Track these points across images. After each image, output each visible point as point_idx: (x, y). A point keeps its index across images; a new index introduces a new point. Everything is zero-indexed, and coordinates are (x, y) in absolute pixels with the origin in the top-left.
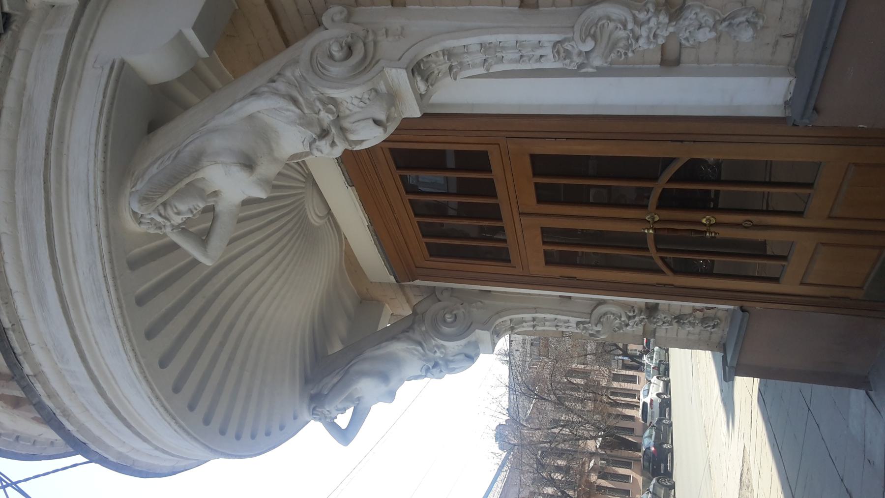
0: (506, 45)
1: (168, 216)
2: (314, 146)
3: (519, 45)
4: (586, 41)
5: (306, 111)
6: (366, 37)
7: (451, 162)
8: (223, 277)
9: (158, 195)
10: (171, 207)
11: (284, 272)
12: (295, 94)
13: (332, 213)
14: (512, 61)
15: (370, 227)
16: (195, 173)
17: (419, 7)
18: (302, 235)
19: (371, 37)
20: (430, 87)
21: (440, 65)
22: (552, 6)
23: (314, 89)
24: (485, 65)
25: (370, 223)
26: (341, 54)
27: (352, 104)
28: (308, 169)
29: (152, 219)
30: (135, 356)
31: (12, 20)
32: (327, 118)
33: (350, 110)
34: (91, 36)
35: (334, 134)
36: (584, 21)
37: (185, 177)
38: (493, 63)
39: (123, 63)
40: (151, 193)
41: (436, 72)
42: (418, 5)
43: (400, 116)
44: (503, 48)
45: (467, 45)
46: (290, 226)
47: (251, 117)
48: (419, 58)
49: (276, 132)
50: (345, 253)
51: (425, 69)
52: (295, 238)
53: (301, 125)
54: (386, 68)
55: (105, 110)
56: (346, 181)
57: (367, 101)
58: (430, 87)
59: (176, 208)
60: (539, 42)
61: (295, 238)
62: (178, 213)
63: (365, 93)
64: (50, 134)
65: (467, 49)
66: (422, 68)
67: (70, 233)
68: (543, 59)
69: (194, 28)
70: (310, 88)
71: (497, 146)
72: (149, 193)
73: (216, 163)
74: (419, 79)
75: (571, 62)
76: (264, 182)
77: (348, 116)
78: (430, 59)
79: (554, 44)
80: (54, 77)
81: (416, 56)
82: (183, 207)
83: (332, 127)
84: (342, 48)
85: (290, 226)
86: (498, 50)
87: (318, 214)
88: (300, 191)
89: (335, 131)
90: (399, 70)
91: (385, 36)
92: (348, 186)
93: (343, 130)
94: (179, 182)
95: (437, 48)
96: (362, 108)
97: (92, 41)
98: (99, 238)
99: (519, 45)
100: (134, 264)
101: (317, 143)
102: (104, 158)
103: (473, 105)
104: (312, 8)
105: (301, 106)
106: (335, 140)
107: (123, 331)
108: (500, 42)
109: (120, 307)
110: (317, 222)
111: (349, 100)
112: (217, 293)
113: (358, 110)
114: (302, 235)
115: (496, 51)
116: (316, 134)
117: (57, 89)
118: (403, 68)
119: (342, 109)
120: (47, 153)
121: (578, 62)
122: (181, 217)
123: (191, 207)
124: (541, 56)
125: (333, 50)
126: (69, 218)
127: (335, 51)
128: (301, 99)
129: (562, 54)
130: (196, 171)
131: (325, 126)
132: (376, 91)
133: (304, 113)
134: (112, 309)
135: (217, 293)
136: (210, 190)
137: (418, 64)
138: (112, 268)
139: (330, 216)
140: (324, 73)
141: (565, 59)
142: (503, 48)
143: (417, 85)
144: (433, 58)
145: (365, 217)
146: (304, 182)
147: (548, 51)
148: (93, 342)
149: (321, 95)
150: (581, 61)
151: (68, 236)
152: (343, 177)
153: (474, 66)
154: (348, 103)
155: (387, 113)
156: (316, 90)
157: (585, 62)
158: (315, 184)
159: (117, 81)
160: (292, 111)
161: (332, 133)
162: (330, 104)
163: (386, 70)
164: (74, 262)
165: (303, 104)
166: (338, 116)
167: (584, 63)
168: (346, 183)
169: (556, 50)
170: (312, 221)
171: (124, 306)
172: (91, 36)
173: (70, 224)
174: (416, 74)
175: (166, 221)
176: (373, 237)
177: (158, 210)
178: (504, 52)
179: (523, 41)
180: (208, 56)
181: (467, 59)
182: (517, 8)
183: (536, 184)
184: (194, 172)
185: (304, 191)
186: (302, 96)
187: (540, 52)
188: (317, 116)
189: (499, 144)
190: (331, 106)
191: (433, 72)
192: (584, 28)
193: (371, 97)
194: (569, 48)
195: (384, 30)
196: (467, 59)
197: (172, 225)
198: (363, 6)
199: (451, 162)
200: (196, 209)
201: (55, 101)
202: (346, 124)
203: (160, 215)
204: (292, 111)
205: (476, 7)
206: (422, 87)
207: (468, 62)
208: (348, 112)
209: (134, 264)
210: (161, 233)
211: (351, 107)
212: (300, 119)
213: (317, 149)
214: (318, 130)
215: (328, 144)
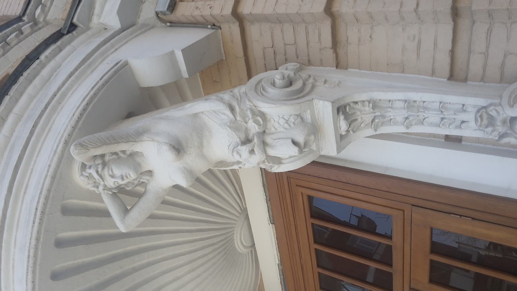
0: (429, 106)
1: (103, 176)
2: (235, 149)
3: (442, 107)
4: (514, 106)
5: (238, 118)
6: (307, 80)
7: (370, 278)
8: (132, 245)
9: (93, 146)
10: (108, 168)
11: (198, 276)
12: (235, 104)
13: (255, 247)
14: (431, 124)
15: (280, 265)
16: (133, 143)
17: (358, 70)
18: (223, 253)
19: (311, 80)
20: (351, 132)
21: (364, 114)
22: (480, 81)
23: (250, 101)
24: (406, 121)
25: (281, 262)
26: (281, 81)
27: (278, 123)
28: (246, 205)
29: (90, 174)
30: (33, 288)
31: (77, 29)
32: (253, 128)
33: (275, 129)
34: (117, 47)
35: (255, 143)
36: (514, 90)
37: (123, 142)
38: (414, 123)
39: (126, 64)
40: (88, 142)
41: (359, 120)
42: (358, 69)
43: (319, 152)
44: (425, 108)
45: (392, 100)
46: (215, 240)
47: (196, 115)
48: (348, 100)
49: (211, 132)
50: (259, 288)
51: (350, 113)
52: (216, 252)
53: (230, 127)
54: (315, 100)
55: (97, 87)
56: (270, 218)
57: (292, 125)
58: (351, 132)
59: (112, 171)
60: (463, 105)
61: (216, 252)
62: (112, 176)
63: (292, 116)
64: (55, 95)
65: (392, 104)
66: (348, 110)
67: (32, 169)
68: (464, 125)
69: (183, 51)
70: (247, 100)
71: (402, 212)
72: (86, 141)
73: (153, 140)
74: (342, 117)
75: (493, 131)
76: (189, 172)
77: (273, 133)
78: (356, 106)
79: (478, 110)
80: (78, 63)
81: (344, 97)
82: (117, 172)
83: (255, 137)
84: (284, 78)
85: (215, 240)
86: (420, 110)
87: (243, 241)
88: (234, 218)
89: (257, 141)
90: (326, 103)
91: (323, 83)
92: (270, 223)
93: (264, 144)
94: (115, 143)
95: (364, 97)
96: (286, 129)
97: (116, 50)
98: (46, 176)
99: (442, 107)
100: (66, 211)
101: (239, 147)
102: (78, 118)
103: (387, 168)
104: (276, 64)
105: (236, 114)
106: (255, 150)
107: (31, 262)
108: (424, 102)
109: (38, 239)
110: (241, 249)
111: (276, 119)
112: (135, 270)
113: (281, 129)
114: (223, 253)
115: (419, 111)
116: (240, 139)
117: (76, 69)
118: (330, 101)
119: (269, 126)
120: (46, 108)
121: (500, 131)
122: (114, 180)
123: (124, 174)
124: (463, 122)
125: (275, 77)
126: (37, 157)
127: (277, 79)
128: (237, 109)
129: (485, 122)
130: (135, 141)
131: (250, 137)
132: (302, 119)
133: (236, 119)
134: (30, 239)
135: (135, 270)
136: (146, 168)
137: (345, 107)
138: (45, 204)
139: (253, 249)
140: (263, 94)
141: (486, 127)
142: (425, 108)
143: (339, 123)
144: (359, 106)
145: (278, 255)
146: (240, 213)
147: (470, 117)
148: (11, 265)
149: (254, 107)
150: (504, 131)
151: (30, 171)
152: (268, 213)
153: (396, 124)
154: (275, 121)
155: (305, 138)
156: (251, 102)
157: (508, 132)
158: (247, 218)
159: (116, 72)
160: (227, 116)
161: (254, 142)
162: (259, 116)
163: (315, 101)
164: (25, 193)
165: (238, 113)
166: (264, 132)
167: (507, 133)
168: (269, 220)
169: (480, 114)
170: (236, 245)
171: (41, 240)
172: (117, 47)
173: (35, 162)
174: (341, 113)
175: (100, 179)
176: (280, 276)
177: (97, 168)
178: (426, 112)
179: (447, 103)
180: (188, 77)
181: (390, 114)
182: (446, 80)
183: (432, 261)
184: (132, 141)
185: (237, 219)
186: (239, 107)
187: (463, 117)
188: (246, 125)
189: (404, 211)
190: (259, 119)
191: (357, 120)
192: (514, 96)
193: (296, 122)
194: (494, 113)
195: (323, 80)
196: (390, 114)
197: (105, 186)
198: (314, 66)
199: (370, 278)
200: (127, 178)
201: (70, 76)
202: (269, 139)
203: (97, 172)
204: (227, 116)
205: (408, 75)
206: (343, 125)
207: (390, 116)
208: (273, 130)
209: (66, 211)
210: (97, 192)
211: (277, 125)
212: (230, 122)
213: (237, 152)
214: (243, 137)
215: (247, 150)
